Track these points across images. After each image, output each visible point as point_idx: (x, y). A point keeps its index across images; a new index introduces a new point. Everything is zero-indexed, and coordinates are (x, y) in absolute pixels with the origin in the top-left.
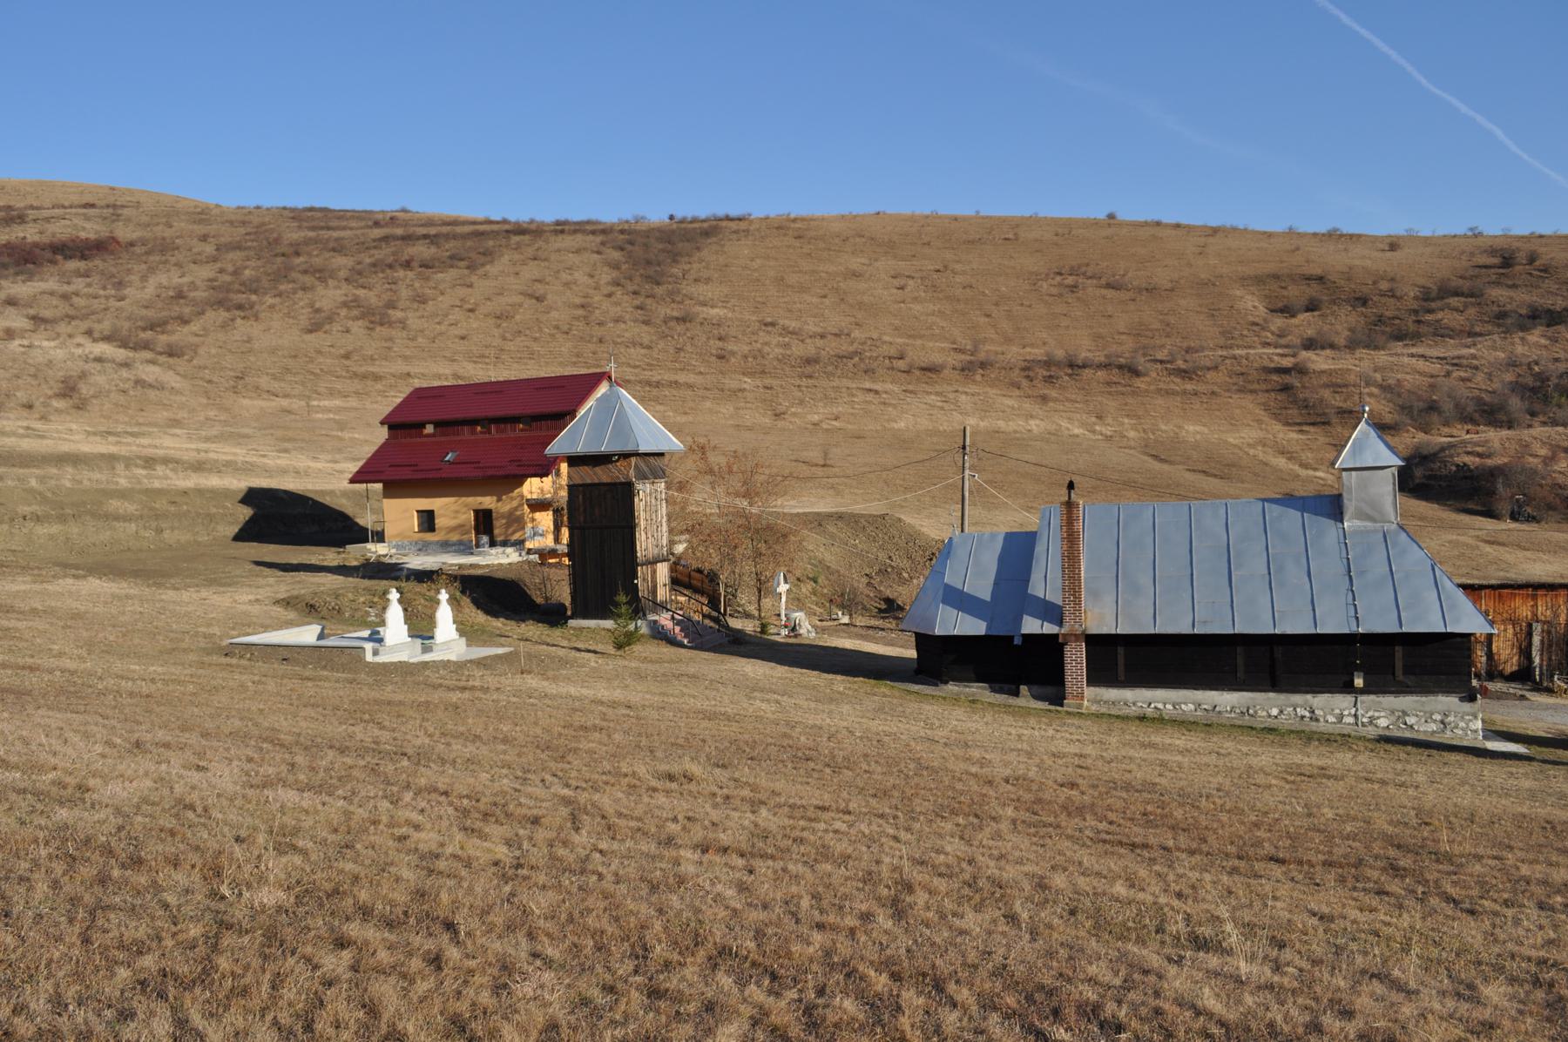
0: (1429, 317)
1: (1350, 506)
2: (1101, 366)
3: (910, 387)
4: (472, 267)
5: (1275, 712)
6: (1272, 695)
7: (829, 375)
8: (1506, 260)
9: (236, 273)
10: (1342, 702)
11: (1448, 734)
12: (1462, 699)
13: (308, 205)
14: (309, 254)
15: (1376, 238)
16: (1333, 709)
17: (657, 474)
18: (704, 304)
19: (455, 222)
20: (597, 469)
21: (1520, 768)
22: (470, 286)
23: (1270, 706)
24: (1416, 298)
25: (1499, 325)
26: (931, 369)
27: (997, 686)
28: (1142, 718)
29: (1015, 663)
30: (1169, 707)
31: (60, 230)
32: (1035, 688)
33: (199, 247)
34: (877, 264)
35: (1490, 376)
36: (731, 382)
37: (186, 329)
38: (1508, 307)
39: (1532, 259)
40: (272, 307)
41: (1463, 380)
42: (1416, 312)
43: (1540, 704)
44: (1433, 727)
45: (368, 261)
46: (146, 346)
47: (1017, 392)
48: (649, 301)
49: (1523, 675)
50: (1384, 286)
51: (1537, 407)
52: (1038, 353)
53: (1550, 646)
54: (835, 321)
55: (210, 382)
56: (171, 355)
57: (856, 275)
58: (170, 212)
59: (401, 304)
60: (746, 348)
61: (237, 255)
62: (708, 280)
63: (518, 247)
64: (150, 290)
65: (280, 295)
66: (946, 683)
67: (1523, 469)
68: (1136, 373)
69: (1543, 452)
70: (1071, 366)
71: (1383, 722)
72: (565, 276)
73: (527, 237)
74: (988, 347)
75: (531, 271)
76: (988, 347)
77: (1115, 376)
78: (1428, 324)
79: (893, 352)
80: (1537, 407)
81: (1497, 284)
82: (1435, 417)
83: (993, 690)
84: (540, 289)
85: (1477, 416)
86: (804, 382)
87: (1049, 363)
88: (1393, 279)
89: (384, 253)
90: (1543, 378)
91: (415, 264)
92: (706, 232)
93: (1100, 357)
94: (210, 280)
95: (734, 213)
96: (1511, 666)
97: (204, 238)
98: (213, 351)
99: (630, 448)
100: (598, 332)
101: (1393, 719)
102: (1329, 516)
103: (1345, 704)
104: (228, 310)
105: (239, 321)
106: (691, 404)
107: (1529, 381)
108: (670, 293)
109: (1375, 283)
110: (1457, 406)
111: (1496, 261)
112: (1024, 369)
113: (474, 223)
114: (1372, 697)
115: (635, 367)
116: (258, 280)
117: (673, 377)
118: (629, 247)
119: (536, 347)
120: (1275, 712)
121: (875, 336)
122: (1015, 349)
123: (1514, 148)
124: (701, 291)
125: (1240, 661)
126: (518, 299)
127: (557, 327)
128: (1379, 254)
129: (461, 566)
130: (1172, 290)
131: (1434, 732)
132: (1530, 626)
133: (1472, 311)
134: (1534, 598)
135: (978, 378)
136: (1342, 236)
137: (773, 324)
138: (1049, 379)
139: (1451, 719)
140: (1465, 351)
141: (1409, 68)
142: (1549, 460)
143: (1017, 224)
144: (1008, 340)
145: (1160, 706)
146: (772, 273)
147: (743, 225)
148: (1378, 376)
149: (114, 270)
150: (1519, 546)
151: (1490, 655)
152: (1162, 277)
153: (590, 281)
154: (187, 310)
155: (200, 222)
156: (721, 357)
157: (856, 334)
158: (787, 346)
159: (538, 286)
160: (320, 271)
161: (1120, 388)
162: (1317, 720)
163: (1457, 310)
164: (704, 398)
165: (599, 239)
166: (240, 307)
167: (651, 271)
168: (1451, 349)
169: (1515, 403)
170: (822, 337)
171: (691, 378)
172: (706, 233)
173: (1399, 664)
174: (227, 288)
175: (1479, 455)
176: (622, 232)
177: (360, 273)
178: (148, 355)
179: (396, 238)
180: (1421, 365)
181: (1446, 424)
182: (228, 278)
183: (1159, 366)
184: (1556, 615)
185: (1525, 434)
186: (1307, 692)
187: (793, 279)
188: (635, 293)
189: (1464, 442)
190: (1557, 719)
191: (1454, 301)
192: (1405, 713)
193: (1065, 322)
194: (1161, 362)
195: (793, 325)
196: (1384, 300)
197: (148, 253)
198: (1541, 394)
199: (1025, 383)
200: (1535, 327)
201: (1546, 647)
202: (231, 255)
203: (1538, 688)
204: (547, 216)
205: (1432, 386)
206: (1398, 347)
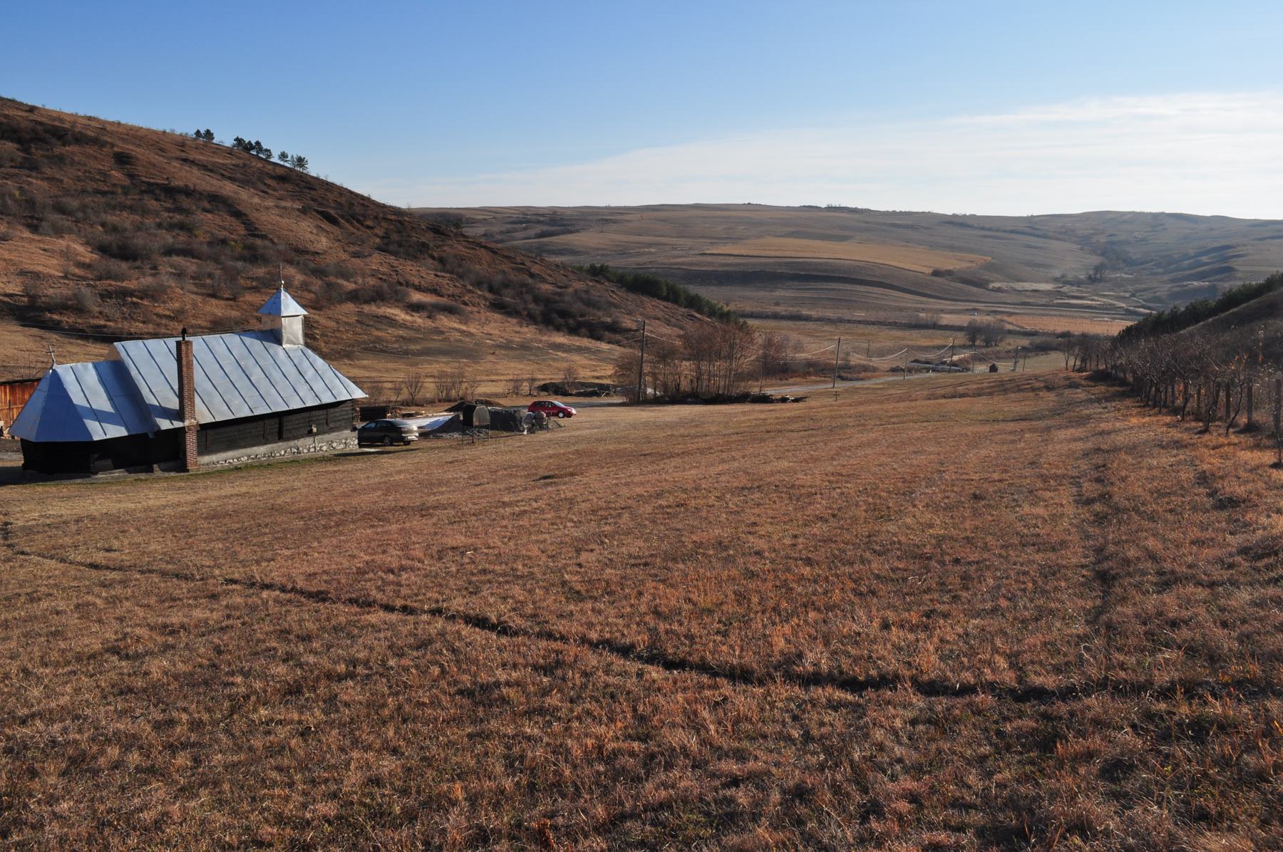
23: (281, 450)
32: (163, 465)
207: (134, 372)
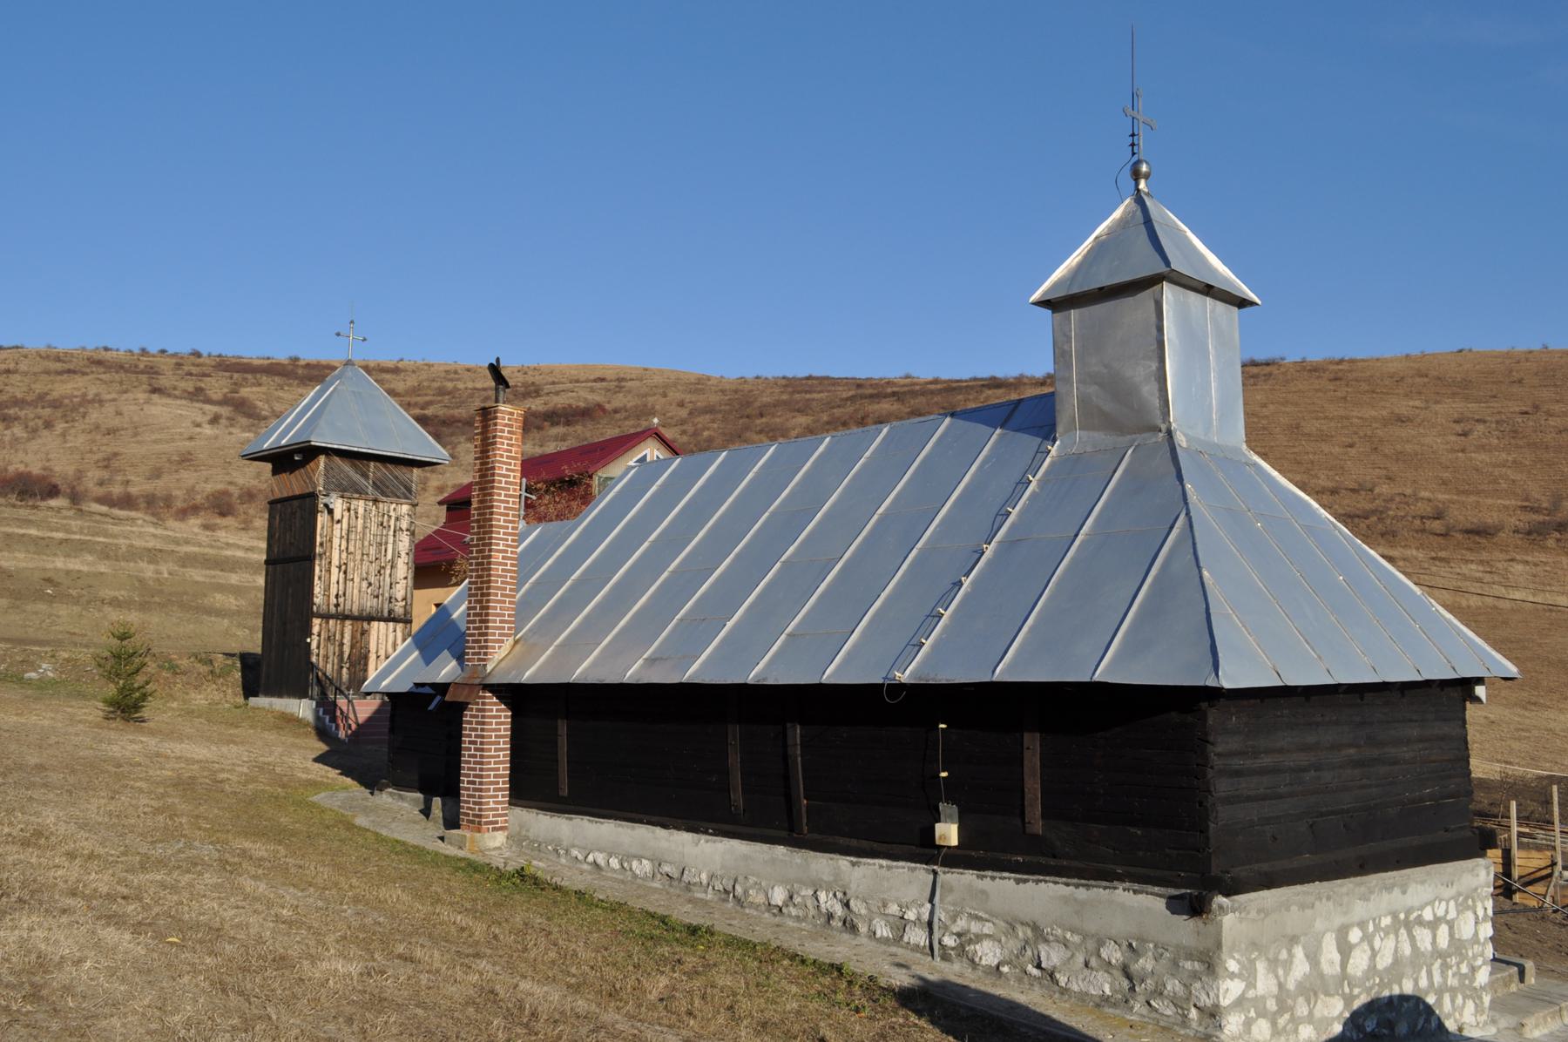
3: (1443, 554)
5: (778, 896)
9: (695, 434)
12: (1174, 905)
26: (1481, 533)
31: (560, 401)
34: (1437, 407)
57: (1401, 420)
79: (1427, 509)
101: (1014, 945)
120: (778, 896)
121: (1409, 491)
125: (734, 760)
139: (1145, 964)
147: (1268, 369)
155: (697, 391)
192: (1039, 934)
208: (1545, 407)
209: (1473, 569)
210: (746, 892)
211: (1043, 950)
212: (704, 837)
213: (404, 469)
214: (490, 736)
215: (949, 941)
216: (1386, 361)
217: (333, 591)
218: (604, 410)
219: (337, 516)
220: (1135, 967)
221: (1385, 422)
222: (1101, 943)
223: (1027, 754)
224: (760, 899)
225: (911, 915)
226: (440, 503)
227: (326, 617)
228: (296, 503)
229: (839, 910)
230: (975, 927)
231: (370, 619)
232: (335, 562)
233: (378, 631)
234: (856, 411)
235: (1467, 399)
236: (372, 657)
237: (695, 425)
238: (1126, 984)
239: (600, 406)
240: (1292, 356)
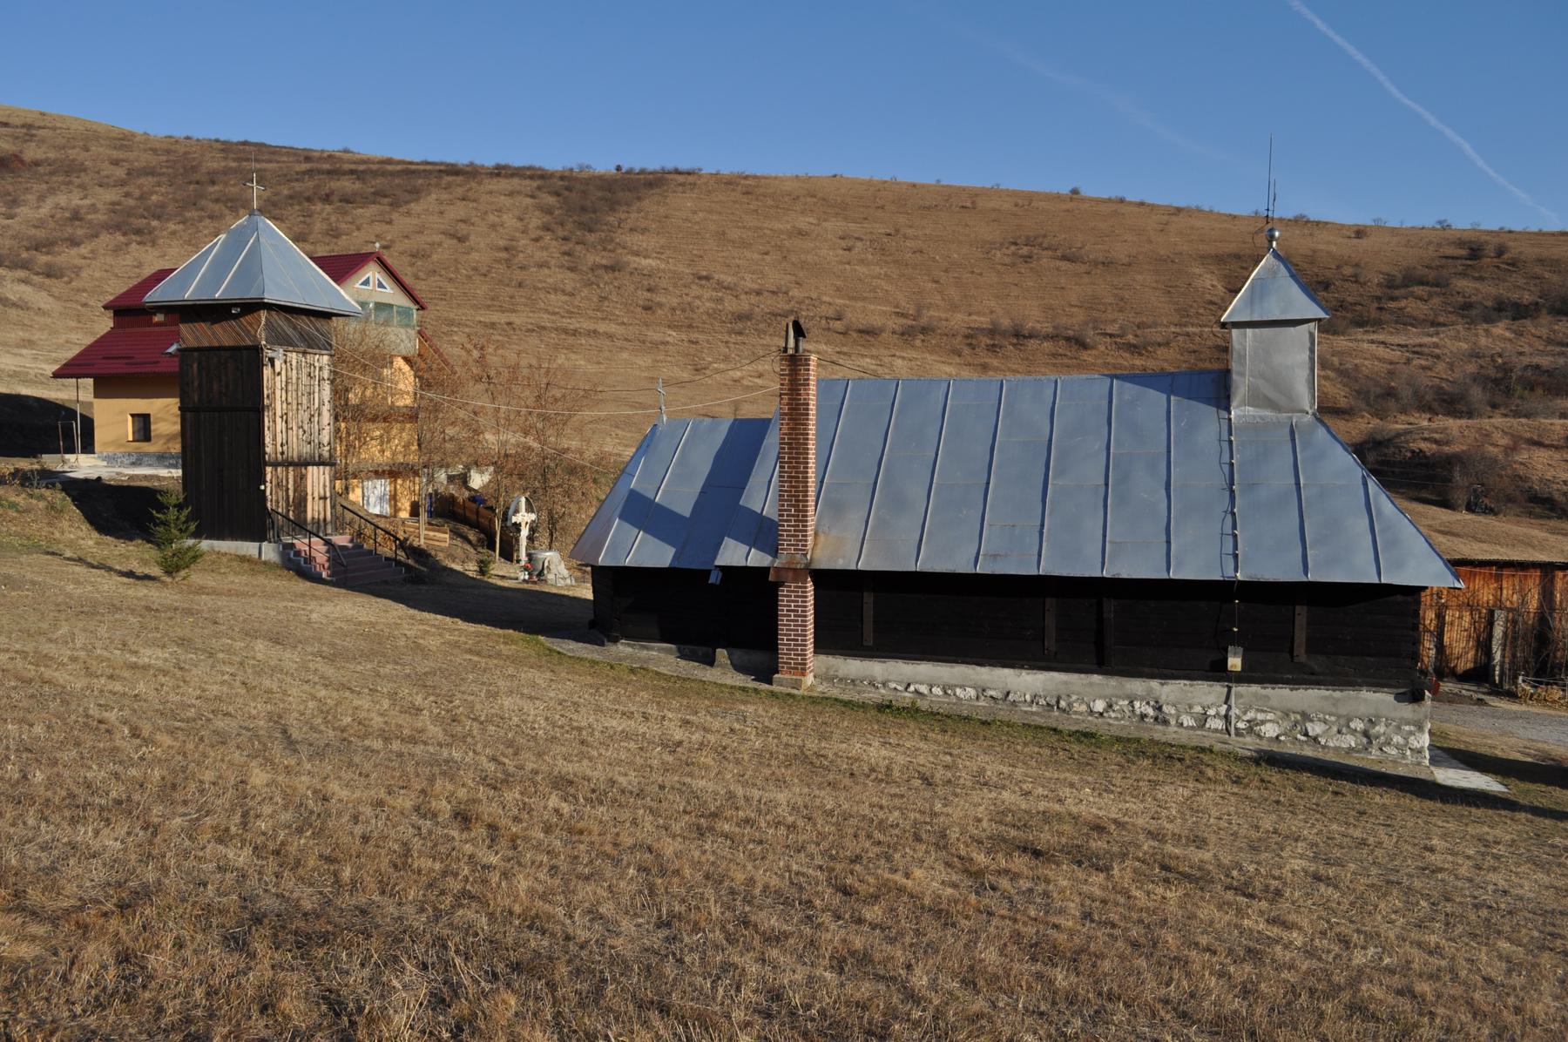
0: (1392, 305)
1: (1241, 386)
2: (1048, 337)
3: (845, 349)
4: (395, 205)
5: (1099, 706)
6: (1096, 678)
7: (760, 333)
8: (1475, 252)
9: (142, 197)
10: (1206, 694)
11: (1375, 753)
12: (1399, 698)
13: (242, 139)
14: (226, 184)
15: (1343, 226)
16: (1189, 705)
17: (310, 344)
18: (637, 254)
19: (389, 161)
20: (217, 327)
21: (1505, 830)
22: (390, 222)
23: (1093, 696)
24: (1379, 285)
25: (1463, 317)
26: (869, 332)
27: (688, 648)
28: (884, 707)
29: (702, 609)
30: (937, 691)
32: (739, 654)
33: (107, 169)
34: (825, 224)
35: (1451, 366)
36: (654, 335)
37: (74, 251)
38: (1474, 299)
39: (1501, 251)
40: (173, 233)
41: (1424, 368)
42: (1379, 299)
43: (1506, 711)
44: (1350, 741)
45: (286, 192)
46: (25, 265)
47: (957, 359)
48: (578, 248)
49: (1480, 675)
50: (1348, 271)
51: (1499, 399)
52: (983, 321)
53: (1515, 639)
54: (774, 278)
55: (85, 305)
56: (48, 276)
57: (801, 234)
58: (90, 137)
59: (312, 238)
60: (675, 301)
61: (147, 182)
62: (644, 231)
63: (448, 187)
64: (45, 211)
65: (184, 223)
66: (615, 641)
67: (1483, 458)
68: (1083, 345)
69: (1504, 441)
70: (1017, 335)
71: (1270, 730)
72: (492, 218)
73: (459, 179)
74: (932, 313)
75: (460, 210)
76: (932, 313)
77: (1062, 347)
78: (1391, 311)
79: (831, 313)
80: (1499, 399)
81: (1464, 275)
82: (1392, 403)
83: (683, 656)
84: (463, 229)
85: (1435, 405)
86: (733, 338)
87: (993, 332)
88: (1357, 265)
89: (308, 185)
90: (1506, 370)
91: (335, 198)
92: (654, 182)
93: (1047, 328)
94: (113, 204)
95: (683, 166)
96: (1465, 664)
97: (116, 163)
98: (97, 275)
99: (252, 294)
100: (519, 275)
101: (1287, 725)
102: (1208, 401)
103: (1211, 699)
104: (125, 234)
105: (134, 246)
106: (606, 354)
107: (1492, 372)
108: (602, 241)
109: (1338, 267)
110: (1415, 393)
111: (1464, 252)
112: (966, 337)
113: (411, 163)
114: (1255, 688)
115: (554, 314)
116: (163, 206)
117: (592, 327)
118: (566, 193)
119: (450, 288)
120: (1099, 706)
121: (814, 296)
122: (959, 316)
123: (1480, 163)
124: (636, 240)
125: (1050, 622)
126: (437, 238)
127: (475, 269)
128: (1345, 241)
129: (131, 477)
130: (1129, 265)
131: (1351, 749)
132: (1491, 613)
133: (1436, 301)
134: (1498, 578)
135: (918, 343)
136: (1308, 222)
137: (707, 278)
138: (992, 349)
139: (1380, 729)
140: (1426, 340)
141: (1382, 78)
142: (1512, 449)
143: (975, 194)
144: (954, 308)
145: (924, 689)
146: (713, 227)
147: (691, 179)
148: (1336, 360)
149: (11, 189)
150: (1475, 538)
151: (1440, 647)
152: (1120, 252)
153: (519, 224)
154: (80, 232)
155: (122, 147)
156: (647, 308)
157: (795, 292)
158: (720, 300)
159: (463, 226)
160: (231, 200)
161: (1066, 361)
162: (1166, 722)
163: (1421, 299)
164: (622, 349)
165: (535, 184)
166: (138, 232)
167: (585, 218)
168: (1413, 337)
169: (1476, 393)
170: (758, 293)
171: (612, 328)
172: (650, 185)
173: (1300, 636)
174: (130, 212)
175: (1436, 442)
176: (562, 178)
177: (274, 205)
178: (21, 274)
179: (320, 172)
180: (1381, 351)
181: (1403, 411)
182: (131, 202)
183: (1108, 339)
184: (1524, 602)
185: (1486, 423)
186: (1152, 676)
187: (734, 234)
188: (565, 239)
189: (1422, 429)
190: (1532, 733)
191: (1419, 290)
192: (1306, 717)
193: (1015, 292)
194: (1111, 336)
195: (728, 279)
196: (1347, 285)
197: (52, 173)
198: (1504, 386)
199: (966, 350)
200: (1500, 320)
201: (1510, 640)
202: (142, 180)
203: (1497, 691)
204: (488, 160)
205: (1391, 373)
206: (1359, 333)
207: (25, 391)
208: (903, 231)
209: (867, 362)
210: (1070, 705)
211: (1309, 726)
212: (1024, 672)
213: (323, 322)
214: (799, 609)
215: (1241, 725)
216: (782, 180)
217: (279, 441)
218: (22, 162)
219: (278, 369)
220: (1374, 731)
221: (790, 235)
222: (1350, 720)
223: (1297, 618)
224: (1083, 708)
225: (1212, 712)
226: (105, 307)
227: (275, 465)
228: (228, 354)
229: (1151, 712)
230: (1260, 716)
231: (306, 464)
232: (279, 413)
233: (312, 472)
234: (317, 187)
235: (846, 219)
236: (310, 498)
237: (140, 187)
238: (1365, 740)
239: (16, 157)
240: (708, 169)
